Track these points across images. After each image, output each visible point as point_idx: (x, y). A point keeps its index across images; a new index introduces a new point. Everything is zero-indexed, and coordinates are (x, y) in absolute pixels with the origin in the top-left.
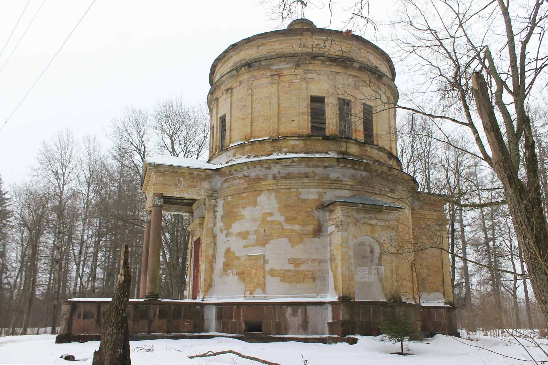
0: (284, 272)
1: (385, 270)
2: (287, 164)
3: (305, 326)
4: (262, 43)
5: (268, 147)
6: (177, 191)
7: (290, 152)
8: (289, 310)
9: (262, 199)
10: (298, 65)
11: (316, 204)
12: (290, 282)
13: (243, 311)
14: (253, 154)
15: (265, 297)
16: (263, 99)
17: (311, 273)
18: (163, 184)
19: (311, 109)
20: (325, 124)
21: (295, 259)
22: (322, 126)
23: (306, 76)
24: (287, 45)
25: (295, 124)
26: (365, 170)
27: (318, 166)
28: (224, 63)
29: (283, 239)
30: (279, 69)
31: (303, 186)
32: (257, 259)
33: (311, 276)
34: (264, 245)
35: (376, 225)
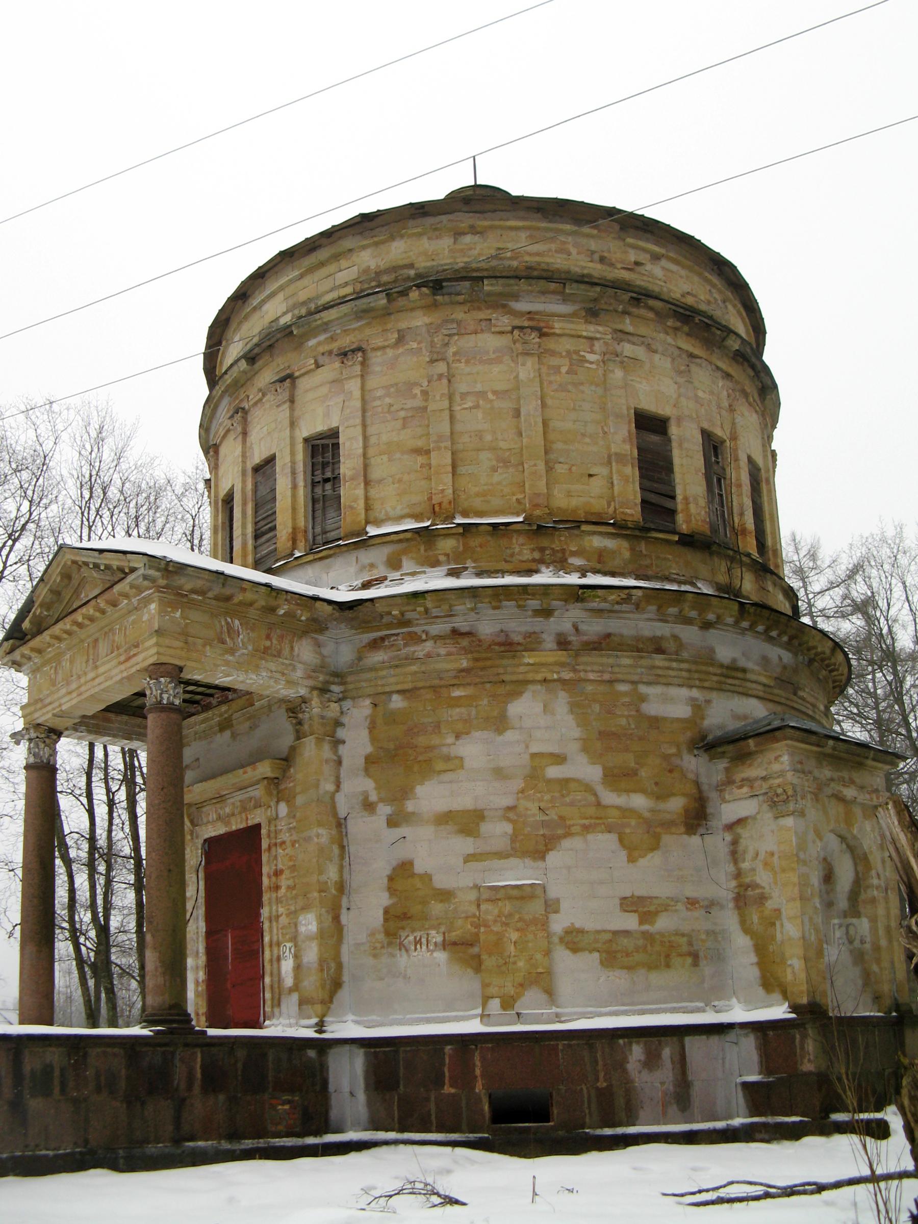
0: (608, 936)
1: (874, 930)
2: (603, 605)
3: (682, 1097)
4: (472, 227)
5: (523, 549)
6: (227, 663)
7: (596, 572)
8: (637, 1052)
9: (525, 708)
10: (592, 314)
11: (689, 734)
12: (630, 968)
13: (483, 1059)
14: (469, 564)
15: (557, 1015)
16: (490, 396)
17: (685, 939)
18: (184, 634)
19: (639, 449)
20: (673, 497)
21: (641, 899)
22: (668, 504)
23: (619, 349)
24: (553, 246)
25: (597, 486)
26: (788, 646)
27: (688, 621)
28: (311, 270)
29: (600, 836)
30: (537, 313)
31: (651, 678)
32: (522, 898)
33: (685, 948)
34: (540, 854)
35: (854, 801)
